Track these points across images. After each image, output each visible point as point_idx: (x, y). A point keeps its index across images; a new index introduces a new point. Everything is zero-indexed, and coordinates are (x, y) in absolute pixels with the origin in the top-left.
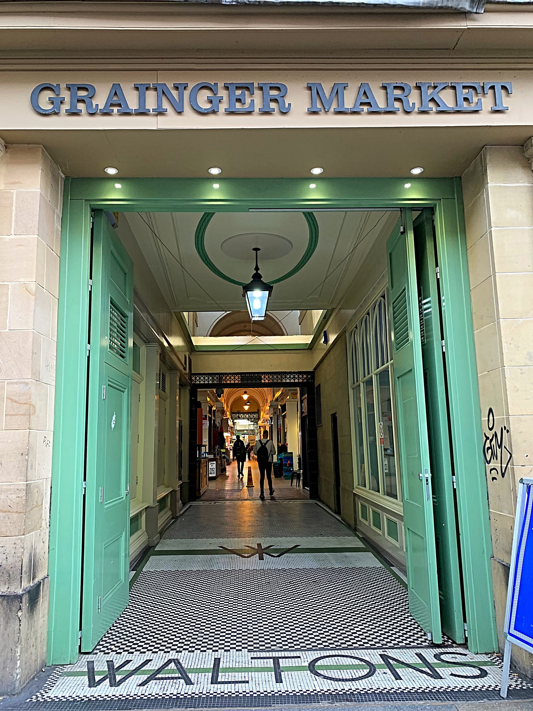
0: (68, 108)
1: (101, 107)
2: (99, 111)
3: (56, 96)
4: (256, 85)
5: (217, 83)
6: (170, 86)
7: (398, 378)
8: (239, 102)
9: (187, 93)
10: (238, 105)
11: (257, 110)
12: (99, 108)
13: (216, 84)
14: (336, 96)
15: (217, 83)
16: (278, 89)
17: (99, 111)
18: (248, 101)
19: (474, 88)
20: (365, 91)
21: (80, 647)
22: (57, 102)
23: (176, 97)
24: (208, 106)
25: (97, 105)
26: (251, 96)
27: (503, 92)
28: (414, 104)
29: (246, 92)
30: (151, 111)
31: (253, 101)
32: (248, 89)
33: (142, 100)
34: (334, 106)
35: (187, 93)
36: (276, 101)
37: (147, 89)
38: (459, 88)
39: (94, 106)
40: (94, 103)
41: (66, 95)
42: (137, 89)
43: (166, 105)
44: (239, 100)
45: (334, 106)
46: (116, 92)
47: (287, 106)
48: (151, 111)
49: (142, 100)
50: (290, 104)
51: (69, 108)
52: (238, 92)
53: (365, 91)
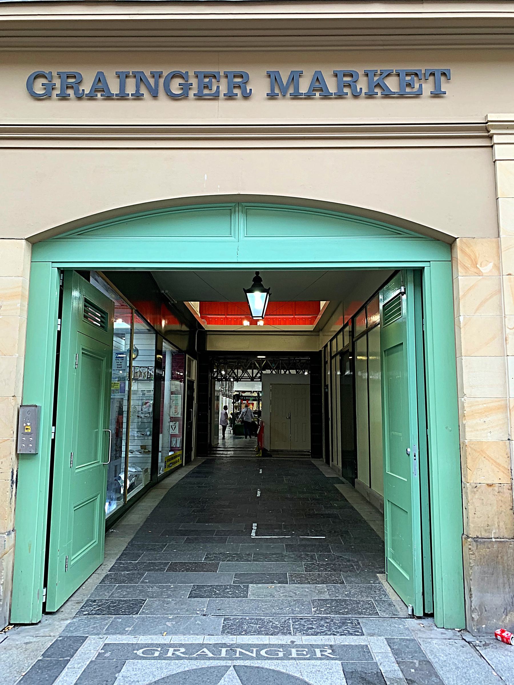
0: (196, 92)
1: (87, 92)
2: (85, 96)
3: (48, 82)
4: (222, 74)
5: (188, 72)
6: (148, 74)
7: (385, 351)
8: (408, 87)
9: (162, 81)
10: (408, 90)
11: (222, 96)
12: (85, 93)
13: (187, 73)
14: (276, 83)
15: (188, 72)
16: (351, 76)
17: (85, 96)
18: (417, 86)
19: (416, 75)
20: (317, 78)
21: (44, 604)
22: (186, 88)
23: (152, 84)
24: (179, 92)
25: (83, 90)
26: (448, 82)
27: (443, 78)
28: (361, 89)
29: (213, 80)
30: (130, 95)
31: (218, 87)
32: (215, 77)
33: (122, 87)
34: (291, 91)
35: (162, 81)
36: (349, 86)
37: (127, 77)
38: (230, 76)
39: (81, 92)
40: (81, 89)
41: (194, 81)
42: (336, 76)
43: (143, 90)
44: (409, 85)
45: (291, 91)
46: (100, 79)
47: (248, 92)
48: (130, 95)
49: (122, 87)
50: (251, 90)
51: (135, 93)
52: (408, 78)
53: (317, 78)
